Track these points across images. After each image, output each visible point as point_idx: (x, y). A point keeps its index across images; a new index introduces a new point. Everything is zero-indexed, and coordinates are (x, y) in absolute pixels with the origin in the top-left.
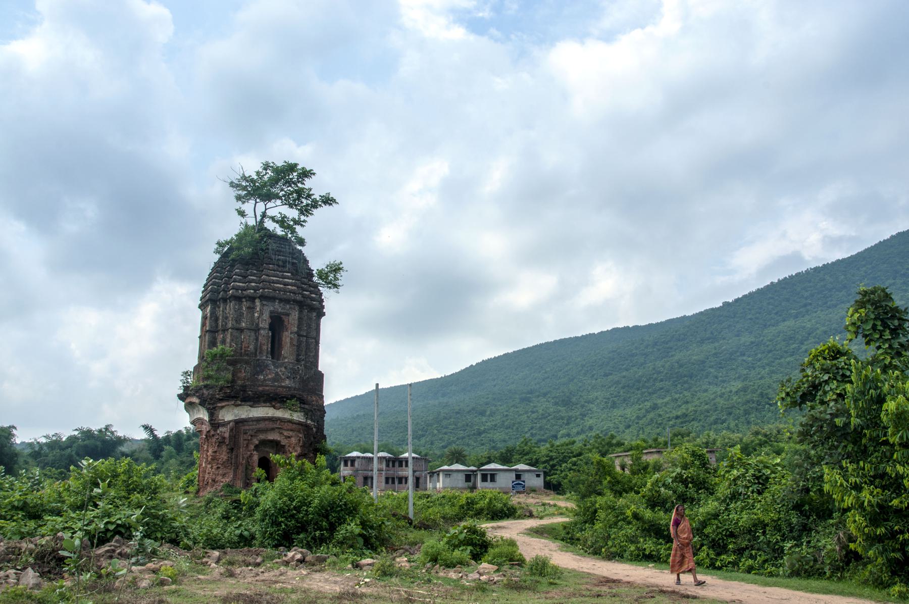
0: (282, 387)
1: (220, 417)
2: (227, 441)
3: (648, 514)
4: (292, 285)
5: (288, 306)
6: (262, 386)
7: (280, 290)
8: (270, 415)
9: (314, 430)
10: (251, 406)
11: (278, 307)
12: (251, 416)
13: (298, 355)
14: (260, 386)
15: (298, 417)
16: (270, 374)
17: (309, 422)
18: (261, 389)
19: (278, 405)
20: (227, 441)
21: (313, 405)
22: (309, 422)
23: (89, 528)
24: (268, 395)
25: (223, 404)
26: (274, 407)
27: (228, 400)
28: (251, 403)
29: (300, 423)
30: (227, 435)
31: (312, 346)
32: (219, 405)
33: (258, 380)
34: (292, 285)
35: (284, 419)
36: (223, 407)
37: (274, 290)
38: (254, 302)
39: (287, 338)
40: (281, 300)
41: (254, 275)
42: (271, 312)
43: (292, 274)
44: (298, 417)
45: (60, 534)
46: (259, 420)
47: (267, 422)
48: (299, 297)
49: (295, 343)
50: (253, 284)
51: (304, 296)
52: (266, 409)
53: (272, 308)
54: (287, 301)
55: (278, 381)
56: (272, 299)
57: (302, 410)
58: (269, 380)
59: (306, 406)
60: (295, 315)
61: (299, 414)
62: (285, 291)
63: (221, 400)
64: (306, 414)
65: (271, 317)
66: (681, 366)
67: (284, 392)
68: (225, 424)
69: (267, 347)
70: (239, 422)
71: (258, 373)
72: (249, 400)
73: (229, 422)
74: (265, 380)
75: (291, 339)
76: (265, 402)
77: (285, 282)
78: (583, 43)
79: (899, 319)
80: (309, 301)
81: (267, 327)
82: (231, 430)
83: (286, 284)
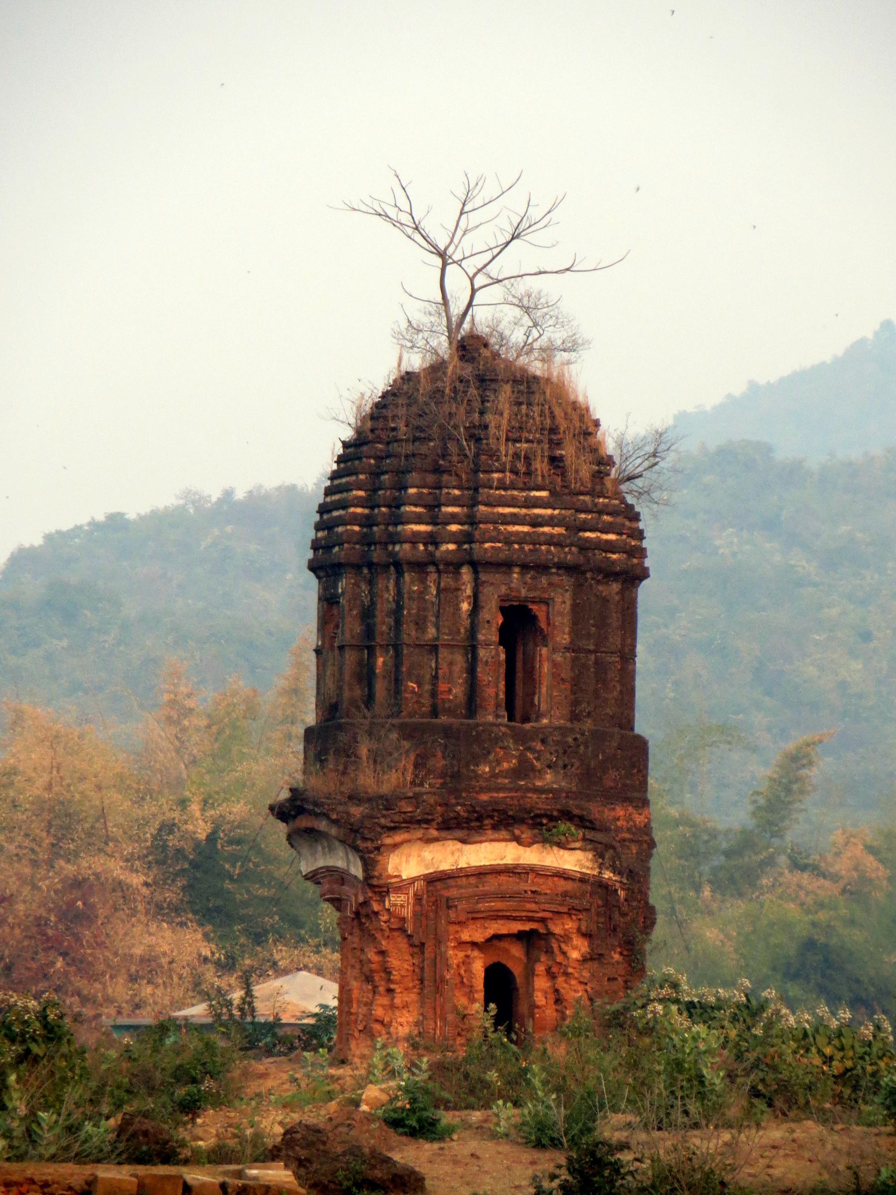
0: (536, 790)
1: (391, 870)
4: (550, 521)
5: (544, 580)
6: (489, 790)
7: (522, 539)
8: (509, 860)
9: (622, 894)
10: (464, 841)
11: (517, 583)
12: (462, 864)
13: (576, 703)
14: (482, 790)
15: (573, 861)
17: (607, 875)
18: (484, 797)
19: (526, 835)
21: (618, 830)
22: (607, 875)
23: (7, 866)
24: (504, 812)
25: (398, 838)
26: (518, 840)
28: (460, 834)
30: (407, 912)
31: (613, 675)
32: (388, 841)
33: (477, 777)
34: (550, 521)
35: (544, 868)
36: (396, 846)
37: (508, 542)
38: (457, 573)
39: (549, 661)
40: (525, 567)
41: (455, 502)
42: (503, 599)
43: (553, 493)
44: (573, 861)
46: (481, 873)
47: (503, 878)
48: (570, 555)
49: (566, 674)
50: (454, 528)
51: (585, 547)
52: (499, 847)
53: (503, 589)
54: (542, 568)
55: (526, 777)
56: (505, 566)
57: (589, 844)
59: (599, 836)
60: (562, 602)
61: (579, 854)
62: (535, 541)
64: (599, 855)
65: (503, 610)
67: (538, 802)
68: (402, 886)
69: (493, 687)
70: (435, 880)
72: (459, 826)
73: (413, 880)
74: (494, 776)
75: (555, 664)
76: (495, 828)
77: (522, 517)
78: (317, 512)
80: (599, 555)
81: (495, 638)
82: (418, 899)
83: (535, 522)
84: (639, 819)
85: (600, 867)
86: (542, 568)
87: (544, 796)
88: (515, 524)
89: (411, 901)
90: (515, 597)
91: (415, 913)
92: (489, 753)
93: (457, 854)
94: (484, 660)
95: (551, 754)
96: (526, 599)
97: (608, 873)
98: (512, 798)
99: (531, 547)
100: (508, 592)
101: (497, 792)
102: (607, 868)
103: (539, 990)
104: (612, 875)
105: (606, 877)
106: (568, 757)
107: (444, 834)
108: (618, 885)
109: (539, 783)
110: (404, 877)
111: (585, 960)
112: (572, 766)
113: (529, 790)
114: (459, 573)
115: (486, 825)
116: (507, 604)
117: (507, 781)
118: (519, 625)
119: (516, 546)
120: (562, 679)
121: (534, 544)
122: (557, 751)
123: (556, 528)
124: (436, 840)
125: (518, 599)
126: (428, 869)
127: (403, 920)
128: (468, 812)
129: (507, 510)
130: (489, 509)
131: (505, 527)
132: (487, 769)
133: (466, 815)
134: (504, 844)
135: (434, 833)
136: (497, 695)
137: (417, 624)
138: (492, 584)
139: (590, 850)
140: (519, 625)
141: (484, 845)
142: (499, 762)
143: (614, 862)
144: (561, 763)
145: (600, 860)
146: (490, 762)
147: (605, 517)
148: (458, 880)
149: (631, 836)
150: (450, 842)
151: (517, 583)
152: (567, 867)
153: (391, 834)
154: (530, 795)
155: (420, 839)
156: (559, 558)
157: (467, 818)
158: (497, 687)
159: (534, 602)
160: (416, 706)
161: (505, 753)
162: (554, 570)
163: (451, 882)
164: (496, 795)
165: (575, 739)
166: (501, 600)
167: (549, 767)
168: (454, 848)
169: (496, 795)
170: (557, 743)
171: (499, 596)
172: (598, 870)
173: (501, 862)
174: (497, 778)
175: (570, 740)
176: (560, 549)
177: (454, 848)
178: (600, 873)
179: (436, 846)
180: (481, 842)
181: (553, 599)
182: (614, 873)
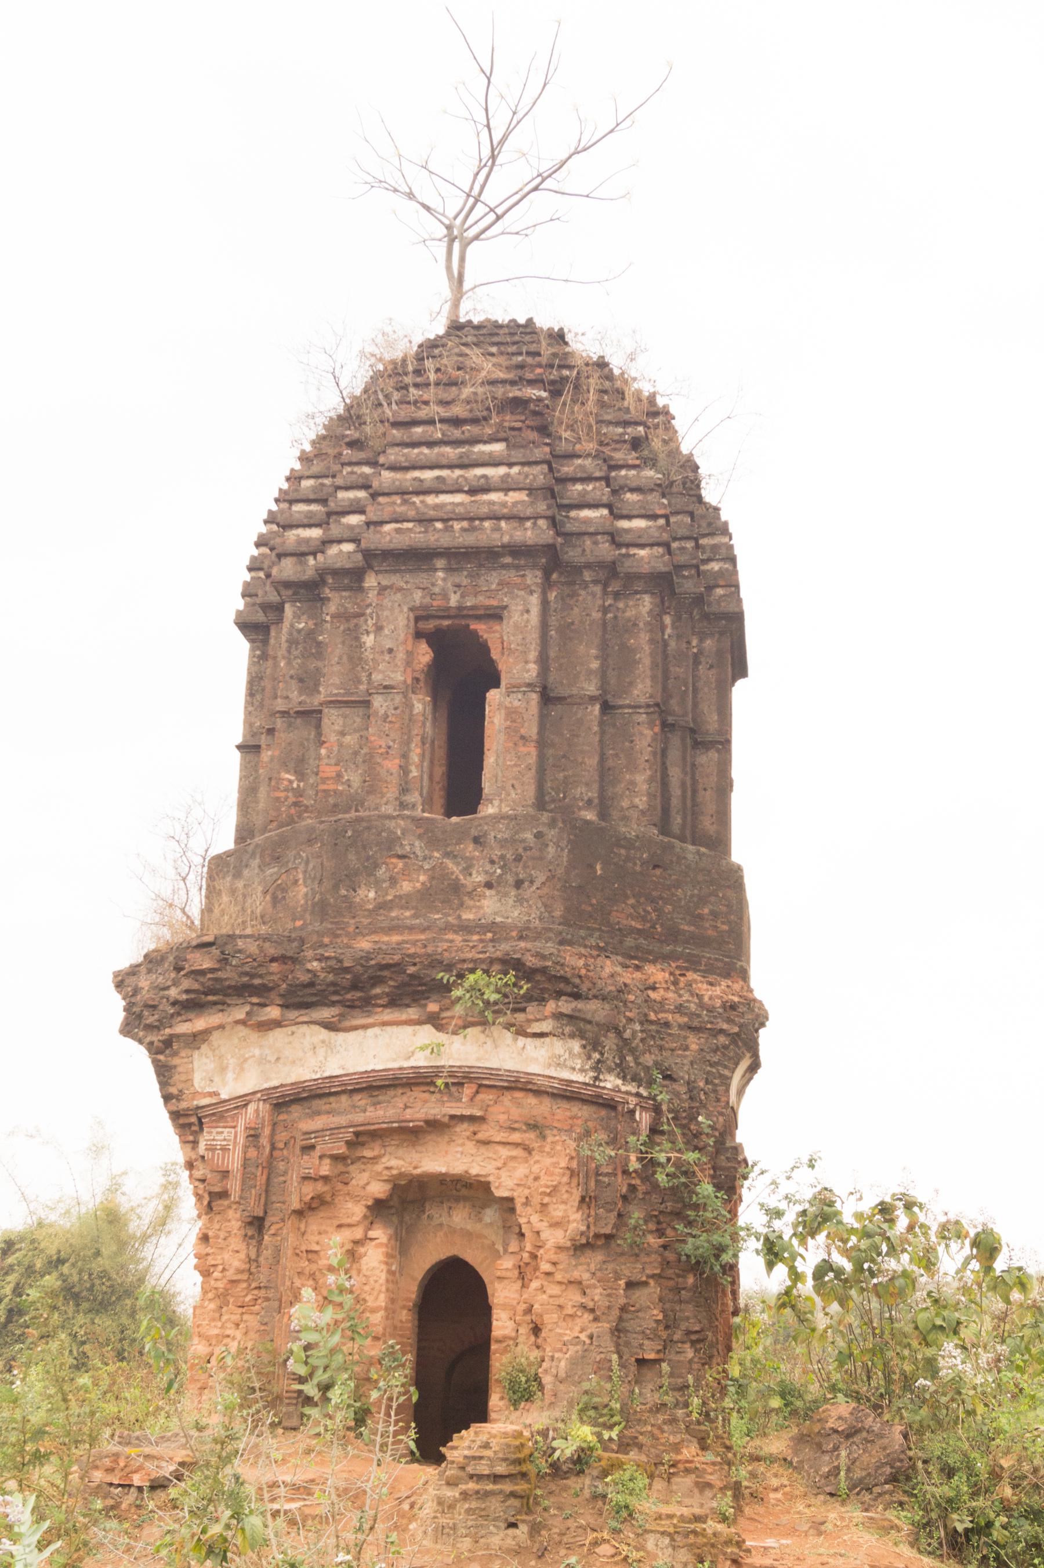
0: (466, 928)
1: (199, 1082)
2: (234, 1186)
3: (385, 404)
8: (421, 1060)
10: (329, 1026)
12: (333, 1069)
14: (359, 932)
15: (545, 1056)
16: (405, 873)
17: (611, 1082)
18: (364, 944)
20: (234, 1186)
22: (611, 1082)
25: (200, 1023)
27: (222, 1005)
28: (325, 1013)
29: (567, 1094)
30: (234, 1162)
32: (183, 1028)
37: (425, 521)
42: (421, 615)
45: (224, 1454)
49: (531, 729)
53: (418, 596)
57: (575, 1025)
58: (403, 902)
59: (593, 1008)
61: (558, 1046)
63: (192, 1005)
64: (593, 1045)
66: (901, 1504)
70: (287, 1100)
71: (350, 879)
73: (243, 1101)
74: (383, 906)
76: (394, 1002)
79: (794, 1413)
82: (253, 1136)
84: (715, 992)
85: (597, 1068)
86: (485, 557)
87: (476, 937)
88: (438, 492)
89: (241, 1140)
90: (439, 609)
91: (246, 1162)
92: (377, 866)
93: (321, 1052)
94: (382, 712)
95: (492, 862)
96: (461, 612)
97: (612, 1078)
98: (414, 943)
99: (465, 524)
100: (428, 600)
101: (387, 934)
102: (610, 1070)
103: (505, 1307)
104: (619, 1082)
105: (609, 1085)
106: (525, 867)
107: (292, 1014)
108: (633, 1101)
109: (468, 916)
110: (224, 1096)
111: (580, 1247)
112: (532, 882)
113: (448, 928)
114: (361, 589)
115: (377, 997)
116: (430, 625)
117: (408, 914)
118: (460, 673)
119: (439, 525)
120: (523, 737)
121: (471, 519)
122: (502, 857)
123: (511, 493)
124: (277, 1024)
125: (445, 613)
126: (268, 1079)
127: (225, 1174)
128: (332, 970)
129: (428, 475)
130: (398, 476)
131: (421, 498)
132: (372, 895)
133: (331, 977)
134: (409, 1029)
135: (273, 1012)
136: (405, 770)
137: (301, 680)
138: (400, 589)
139: (572, 1036)
140: (460, 673)
141: (370, 1032)
142: (393, 881)
143: (622, 1058)
144: (510, 879)
145: (596, 1056)
146: (377, 883)
147: (628, 495)
148: (332, 1099)
149: (686, 1019)
150: (304, 1028)
151: (447, 589)
152: (534, 1068)
153: (191, 1015)
154: (450, 936)
155: (243, 1022)
156: (511, 536)
157: (333, 984)
158: (405, 756)
159: (478, 618)
160: (293, 811)
161: (406, 865)
162: (508, 560)
163: (317, 1104)
164: (386, 939)
165: (539, 835)
166: (417, 619)
167: (489, 885)
168: (316, 1040)
169: (386, 939)
170: (503, 843)
171: (411, 609)
172: (592, 1074)
173: (406, 1064)
174: (391, 909)
175: (528, 836)
176: (516, 524)
177: (316, 1040)
178: (596, 1078)
179: (277, 1036)
180: (365, 1027)
181: (506, 607)
182: (624, 1078)
